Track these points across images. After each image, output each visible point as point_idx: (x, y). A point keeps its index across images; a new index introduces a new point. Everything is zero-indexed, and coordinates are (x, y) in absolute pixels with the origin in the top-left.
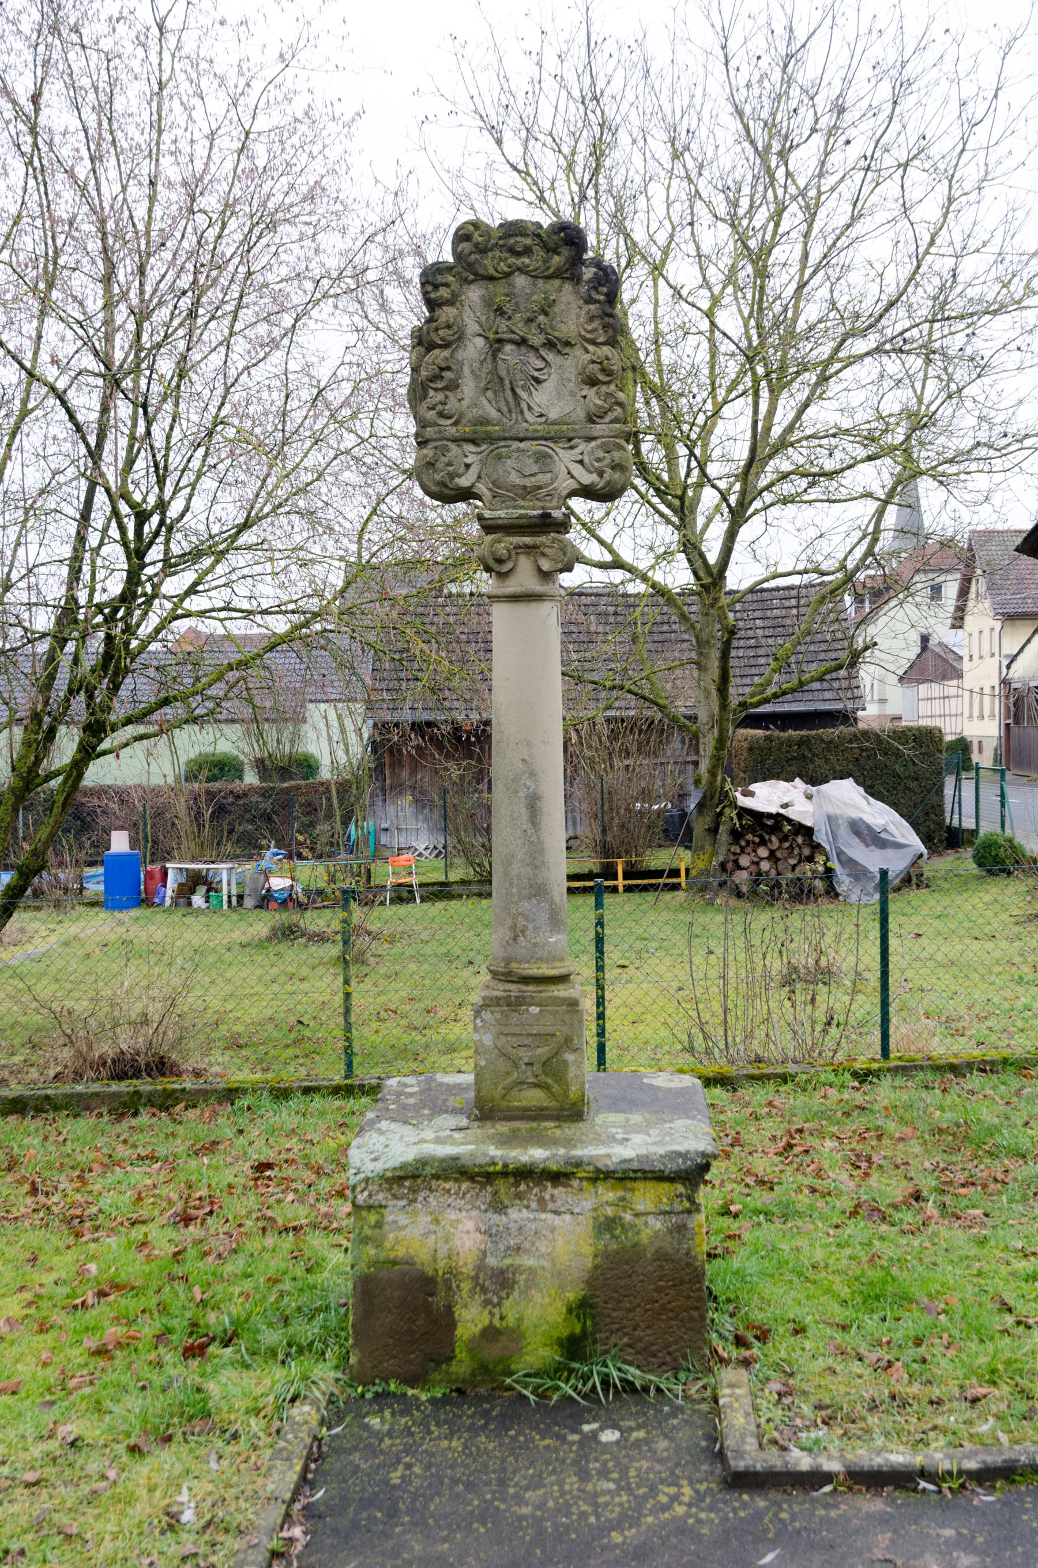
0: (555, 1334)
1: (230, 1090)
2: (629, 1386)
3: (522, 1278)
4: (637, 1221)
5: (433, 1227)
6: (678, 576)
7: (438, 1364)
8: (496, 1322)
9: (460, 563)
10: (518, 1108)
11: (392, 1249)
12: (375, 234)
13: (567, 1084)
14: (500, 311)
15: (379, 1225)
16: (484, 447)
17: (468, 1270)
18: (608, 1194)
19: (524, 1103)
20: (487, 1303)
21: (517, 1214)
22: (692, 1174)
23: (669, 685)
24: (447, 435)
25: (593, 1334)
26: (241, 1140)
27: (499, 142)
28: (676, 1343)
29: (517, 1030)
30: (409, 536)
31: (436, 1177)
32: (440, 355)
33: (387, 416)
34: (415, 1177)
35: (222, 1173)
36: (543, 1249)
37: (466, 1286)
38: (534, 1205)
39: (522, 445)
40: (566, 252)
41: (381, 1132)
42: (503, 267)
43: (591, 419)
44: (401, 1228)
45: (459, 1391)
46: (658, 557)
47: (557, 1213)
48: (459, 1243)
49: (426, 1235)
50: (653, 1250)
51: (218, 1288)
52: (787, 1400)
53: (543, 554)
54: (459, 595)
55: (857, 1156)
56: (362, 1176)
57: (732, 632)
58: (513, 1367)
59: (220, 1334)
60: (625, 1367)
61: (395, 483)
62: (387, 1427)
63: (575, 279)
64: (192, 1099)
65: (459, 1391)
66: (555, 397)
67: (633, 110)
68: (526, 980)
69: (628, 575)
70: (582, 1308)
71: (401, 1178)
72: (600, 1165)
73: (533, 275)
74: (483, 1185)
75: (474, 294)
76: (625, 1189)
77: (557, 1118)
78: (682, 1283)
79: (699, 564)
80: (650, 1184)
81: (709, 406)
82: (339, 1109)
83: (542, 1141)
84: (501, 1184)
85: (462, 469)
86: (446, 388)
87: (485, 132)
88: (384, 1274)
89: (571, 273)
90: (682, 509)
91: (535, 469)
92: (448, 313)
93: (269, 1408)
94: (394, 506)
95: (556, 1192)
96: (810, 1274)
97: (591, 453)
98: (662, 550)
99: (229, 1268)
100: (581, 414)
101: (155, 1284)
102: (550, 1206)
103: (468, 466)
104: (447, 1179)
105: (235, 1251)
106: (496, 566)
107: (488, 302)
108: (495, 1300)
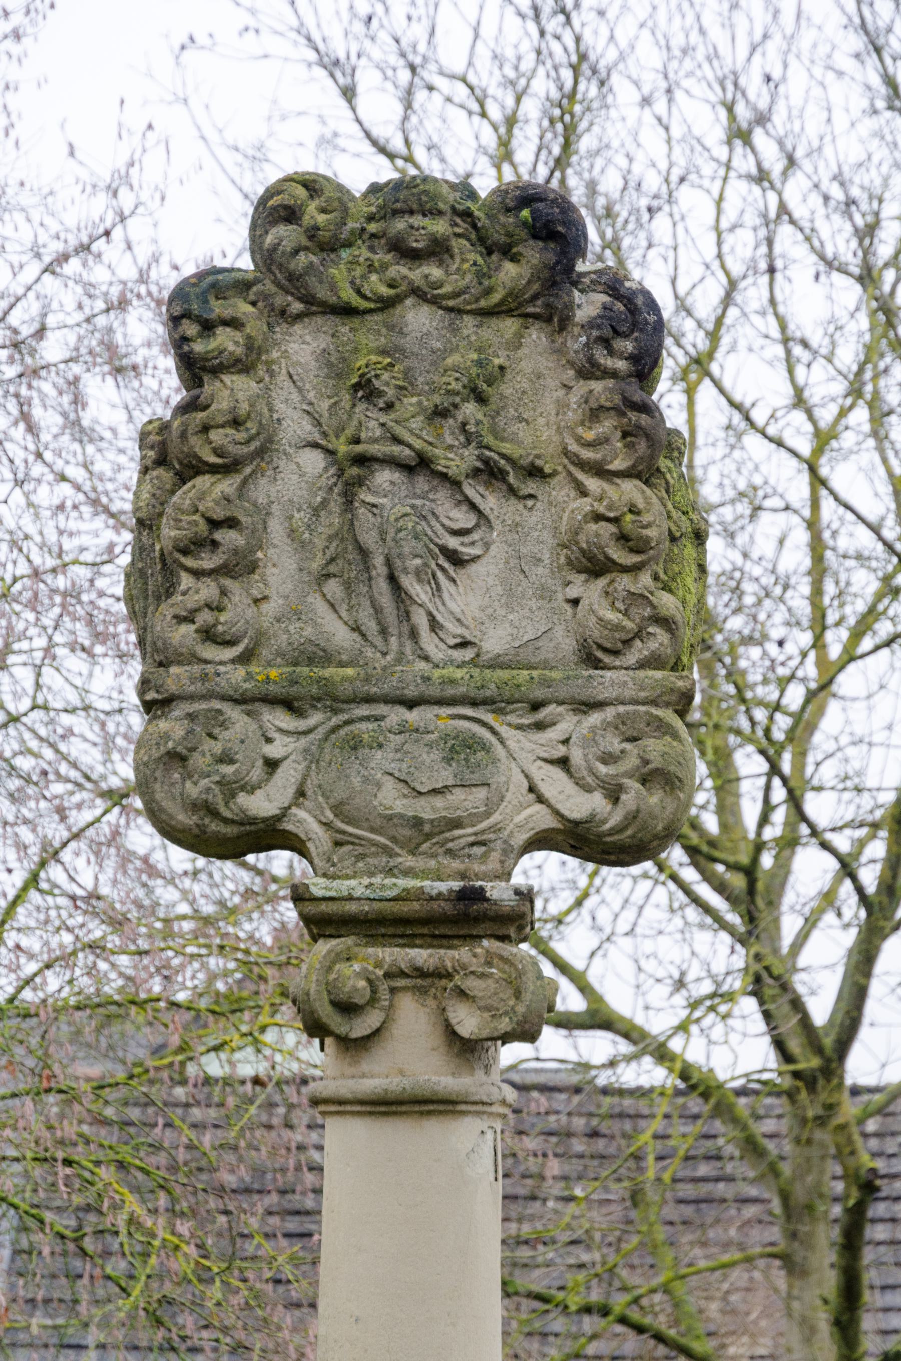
6: (740, 1050)
9: (228, 1007)
12: (64, 258)
14: (366, 390)
16: (315, 718)
23: (714, 1308)
24: (223, 684)
27: (349, 93)
30: (113, 941)
32: (212, 490)
33: (75, 663)
39: (413, 716)
40: (534, 255)
42: (376, 285)
43: (591, 657)
46: (694, 1005)
53: (461, 994)
54: (227, 1082)
57: (869, 1187)
61: (87, 816)
63: (557, 319)
66: (499, 598)
67: (646, 33)
69: (625, 1047)
73: (452, 308)
75: (303, 347)
79: (789, 1024)
81: (810, 670)
85: (257, 773)
86: (224, 570)
87: (322, 73)
89: (544, 304)
90: (751, 899)
91: (445, 776)
92: (231, 391)
94: (81, 870)
97: (590, 740)
98: (707, 988)
100: (564, 643)
103: (272, 765)
106: (334, 1020)
107: (335, 367)
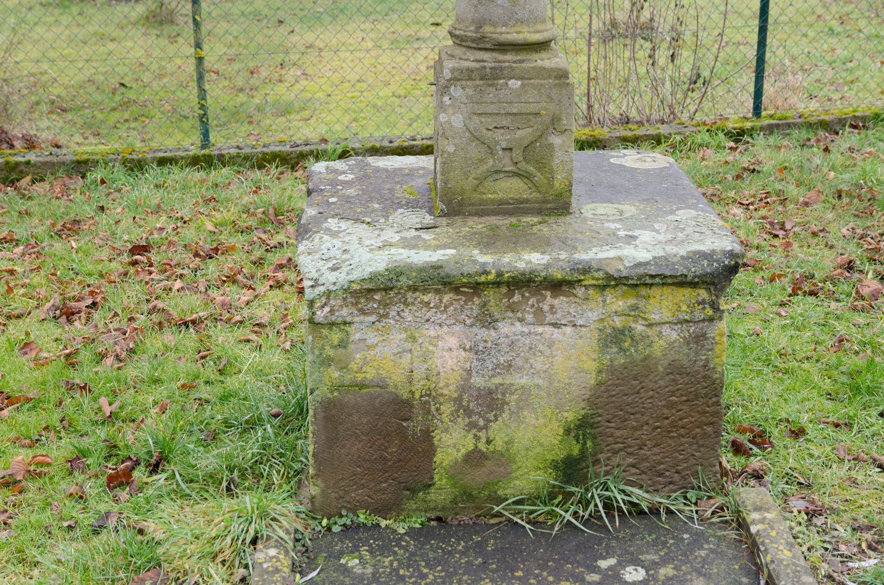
0: (550, 457)
1: (79, 162)
2: (636, 510)
3: (512, 399)
4: (649, 332)
5: (408, 346)
7: (414, 491)
8: (482, 446)
10: (493, 201)
11: (360, 371)
13: (552, 171)
15: (343, 344)
17: (451, 391)
18: (617, 302)
19: (500, 195)
20: (472, 426)
21: (508, 328)
22: (716, 278)
25: (594, 455)
26: (103, 219)
28: (686, 460)
29: (492, 109)
31: (414, 289)
34: (386, 290)
35: (89, 257)
36: (538, 366)
37: (447, 409)
38: (529, 318)
41: (334, 234)
44: (369, 347)
45: (439, 519)
47: (555, 325)
48: (439, 362)
49: (399, 354)
50: (666, 363)
51: (128, 396)
52: (819, 521)
55: (772, 224)
56: (322, 289)
58: (500, 493)
59: (143, 456)
60: (629, 489)
62: (369, 570)
64: (40, 172)
65: (439, 519)
68: (503, 47)
70: (582, 428)
71: (369, 291)
72: (612, 271)
74: (469, 297)
76: (638, 296)
77: (539, 212)
78: (697, 397)
80: (667, 290)
82: (203, 181)
83: (542, 244)
84: (491, 296)
88: (349, 399)
93: (228, 552)
95: (556, 302)
96: (778, 362)
99: (131, 372)
101: (54, 396)
102: (549, 318)
104: (425, 291)
105: (132, 351)
108: (481, 422)
